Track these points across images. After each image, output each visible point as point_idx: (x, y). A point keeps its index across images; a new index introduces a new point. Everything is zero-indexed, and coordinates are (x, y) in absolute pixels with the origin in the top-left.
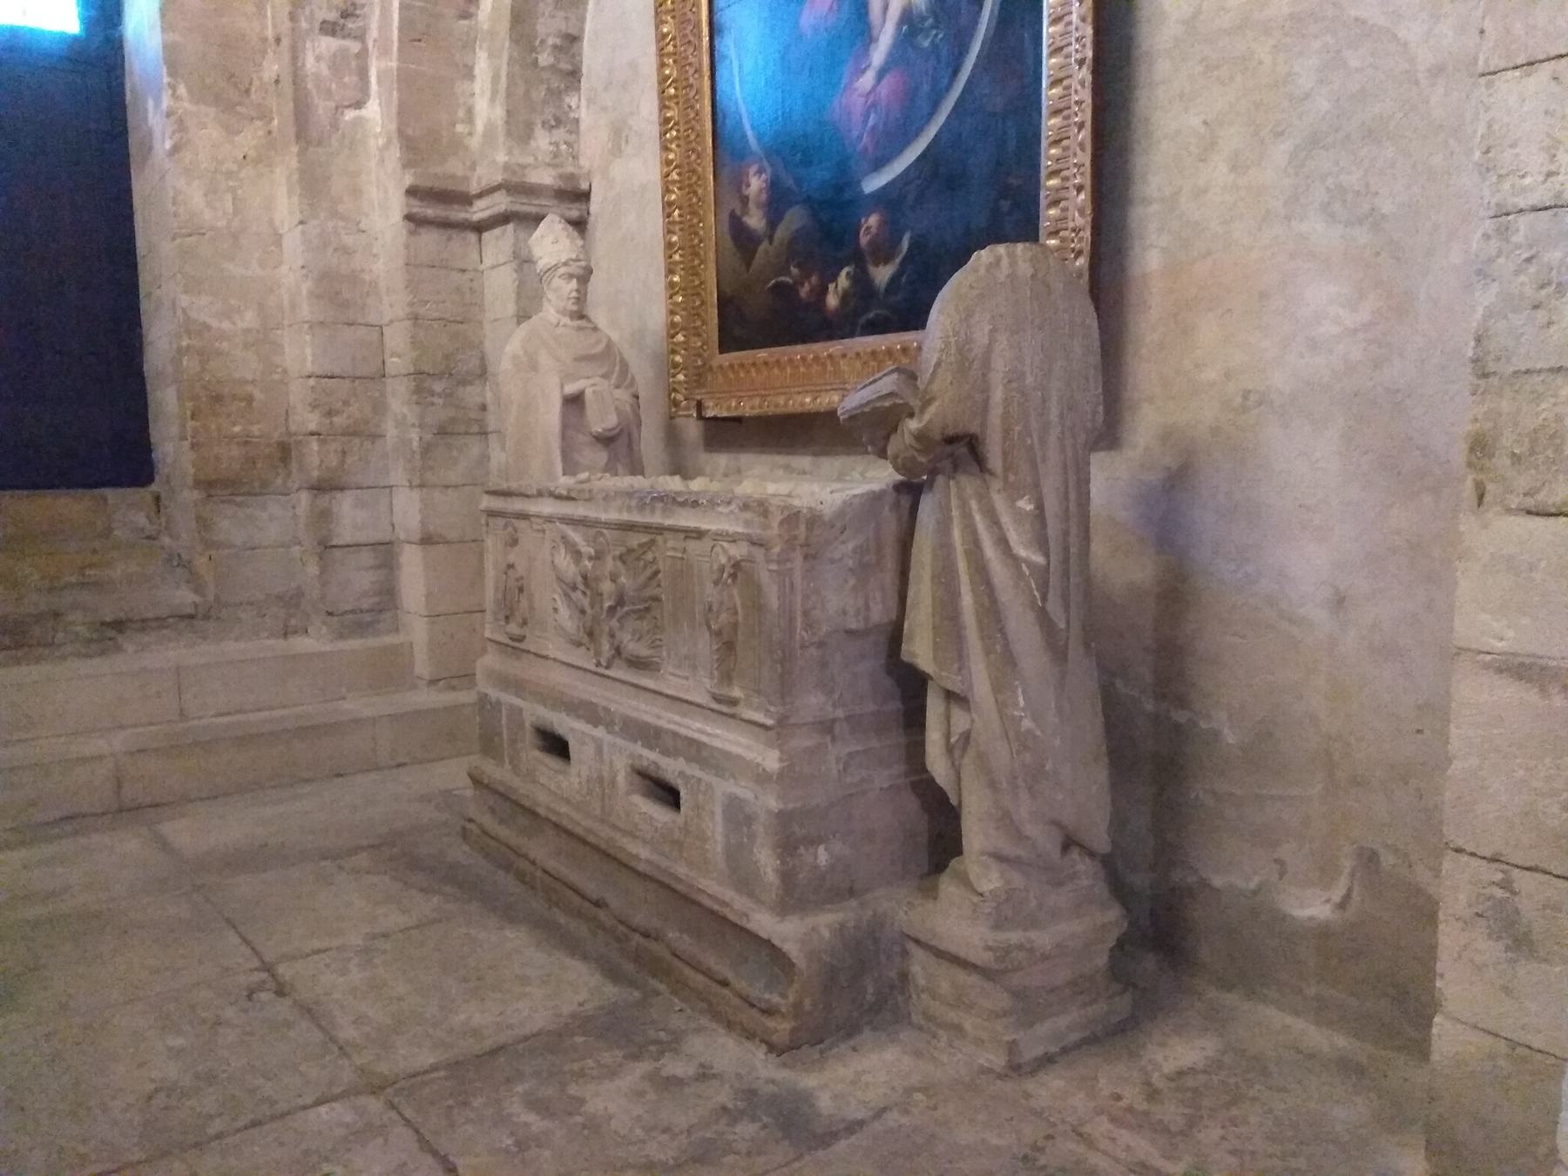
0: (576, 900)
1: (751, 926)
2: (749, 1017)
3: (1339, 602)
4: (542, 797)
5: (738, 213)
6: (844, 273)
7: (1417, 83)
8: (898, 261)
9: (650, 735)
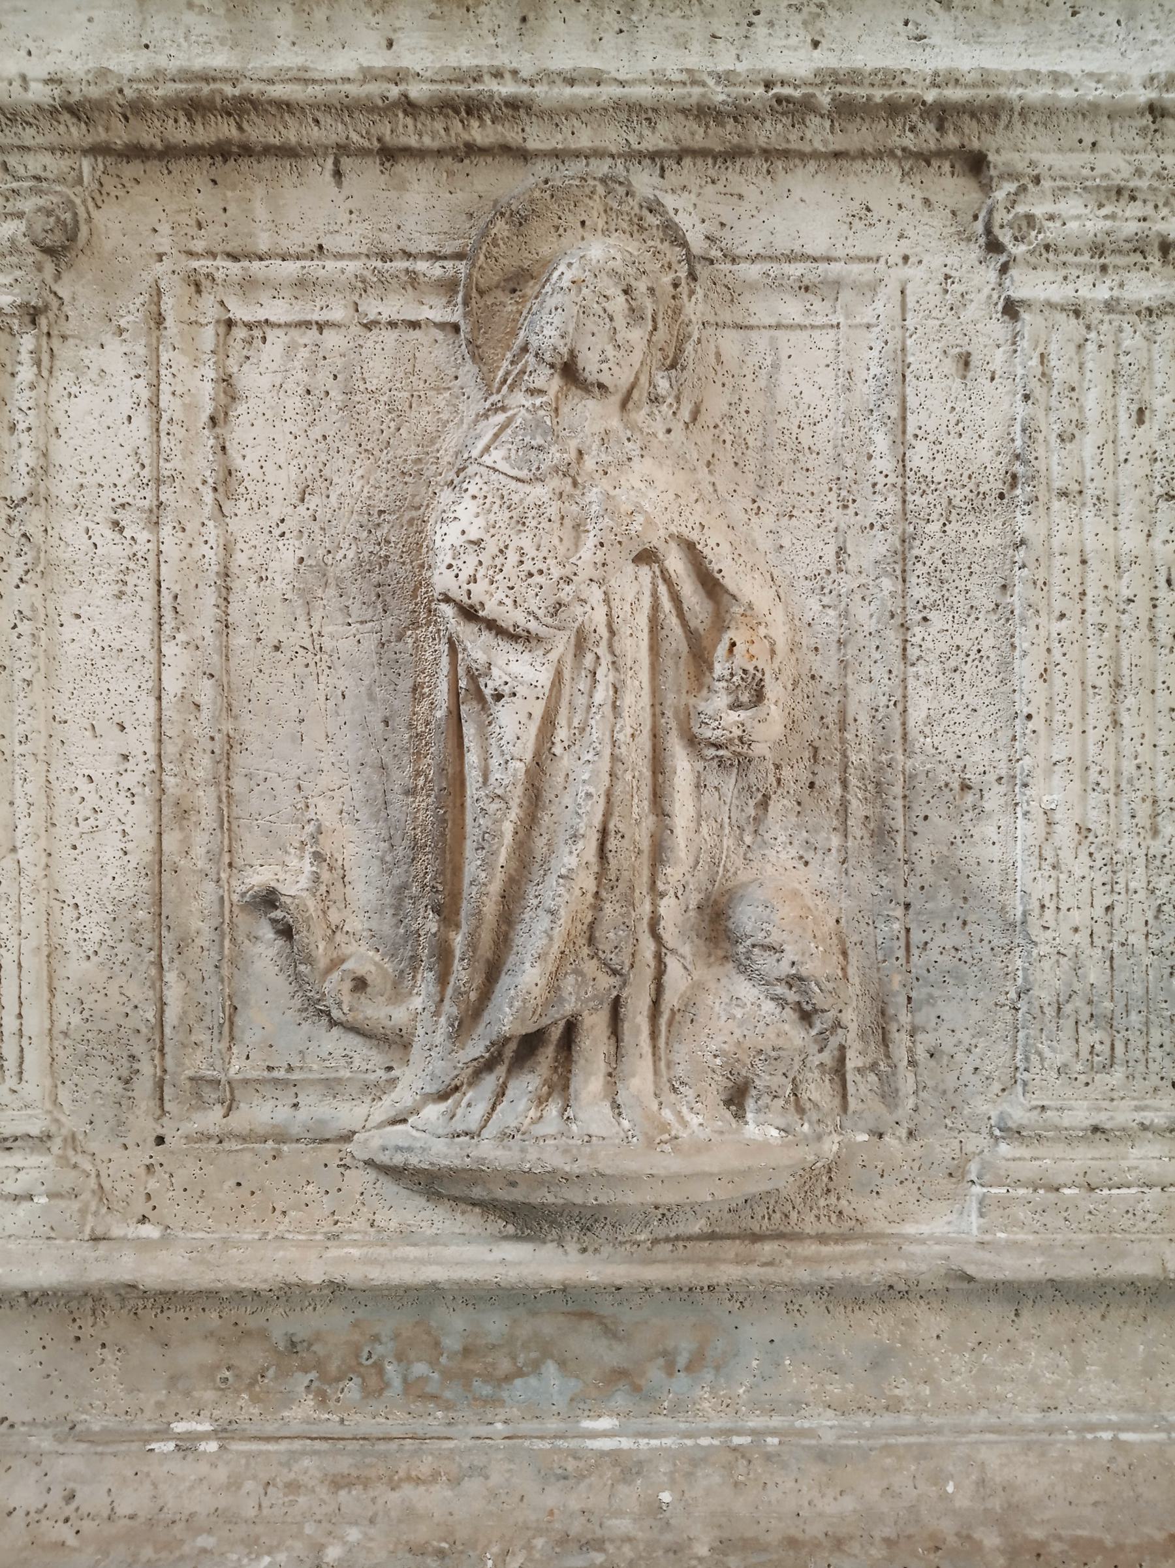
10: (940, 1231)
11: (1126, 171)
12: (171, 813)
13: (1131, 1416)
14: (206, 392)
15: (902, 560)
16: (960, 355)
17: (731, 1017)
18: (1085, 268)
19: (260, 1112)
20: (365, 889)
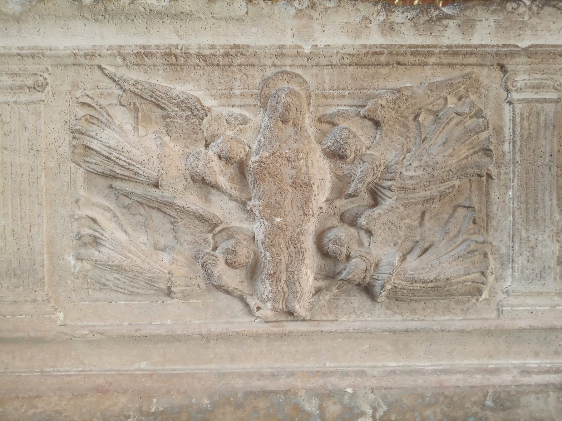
11: (17, 69)
13: (26, 370)
17: (389, 107)
18: (10, 93)
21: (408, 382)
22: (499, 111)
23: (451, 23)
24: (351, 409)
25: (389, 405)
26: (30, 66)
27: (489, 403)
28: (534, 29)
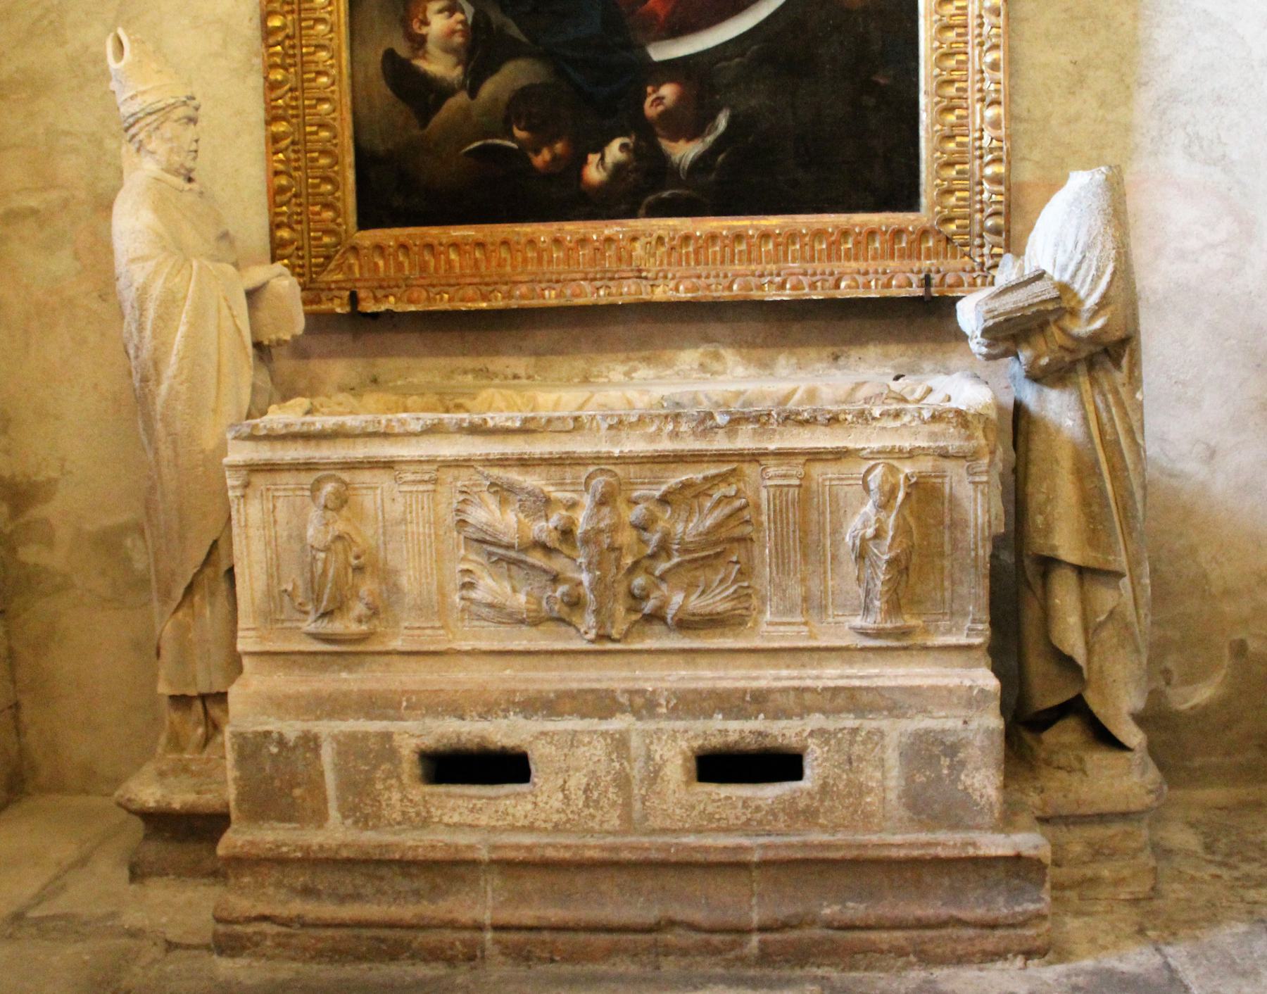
0: (603, 939)
1: (982, 852)
2: (993, 940)
3: (1212, 454)
4: (462, 839)
5: (403, 50)
6: (616, 145)
7: (1252, 67)
8: (710, 139)
9: (691, 704)
10: (397, 644)
12: (270, 576)
14: (271, 506)
15: (384, 534)
16: (466, 543)
19: (288, 624)
20: (301, 591)
21: (693, 685)
22: (757, 491)
23: (720, 431)
24: (651, 701)
25: (678, 699)
26: (426, 467)
27: (748, 698)
28: (781, 434)
